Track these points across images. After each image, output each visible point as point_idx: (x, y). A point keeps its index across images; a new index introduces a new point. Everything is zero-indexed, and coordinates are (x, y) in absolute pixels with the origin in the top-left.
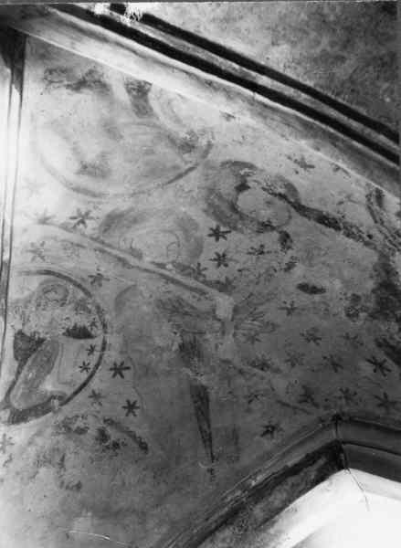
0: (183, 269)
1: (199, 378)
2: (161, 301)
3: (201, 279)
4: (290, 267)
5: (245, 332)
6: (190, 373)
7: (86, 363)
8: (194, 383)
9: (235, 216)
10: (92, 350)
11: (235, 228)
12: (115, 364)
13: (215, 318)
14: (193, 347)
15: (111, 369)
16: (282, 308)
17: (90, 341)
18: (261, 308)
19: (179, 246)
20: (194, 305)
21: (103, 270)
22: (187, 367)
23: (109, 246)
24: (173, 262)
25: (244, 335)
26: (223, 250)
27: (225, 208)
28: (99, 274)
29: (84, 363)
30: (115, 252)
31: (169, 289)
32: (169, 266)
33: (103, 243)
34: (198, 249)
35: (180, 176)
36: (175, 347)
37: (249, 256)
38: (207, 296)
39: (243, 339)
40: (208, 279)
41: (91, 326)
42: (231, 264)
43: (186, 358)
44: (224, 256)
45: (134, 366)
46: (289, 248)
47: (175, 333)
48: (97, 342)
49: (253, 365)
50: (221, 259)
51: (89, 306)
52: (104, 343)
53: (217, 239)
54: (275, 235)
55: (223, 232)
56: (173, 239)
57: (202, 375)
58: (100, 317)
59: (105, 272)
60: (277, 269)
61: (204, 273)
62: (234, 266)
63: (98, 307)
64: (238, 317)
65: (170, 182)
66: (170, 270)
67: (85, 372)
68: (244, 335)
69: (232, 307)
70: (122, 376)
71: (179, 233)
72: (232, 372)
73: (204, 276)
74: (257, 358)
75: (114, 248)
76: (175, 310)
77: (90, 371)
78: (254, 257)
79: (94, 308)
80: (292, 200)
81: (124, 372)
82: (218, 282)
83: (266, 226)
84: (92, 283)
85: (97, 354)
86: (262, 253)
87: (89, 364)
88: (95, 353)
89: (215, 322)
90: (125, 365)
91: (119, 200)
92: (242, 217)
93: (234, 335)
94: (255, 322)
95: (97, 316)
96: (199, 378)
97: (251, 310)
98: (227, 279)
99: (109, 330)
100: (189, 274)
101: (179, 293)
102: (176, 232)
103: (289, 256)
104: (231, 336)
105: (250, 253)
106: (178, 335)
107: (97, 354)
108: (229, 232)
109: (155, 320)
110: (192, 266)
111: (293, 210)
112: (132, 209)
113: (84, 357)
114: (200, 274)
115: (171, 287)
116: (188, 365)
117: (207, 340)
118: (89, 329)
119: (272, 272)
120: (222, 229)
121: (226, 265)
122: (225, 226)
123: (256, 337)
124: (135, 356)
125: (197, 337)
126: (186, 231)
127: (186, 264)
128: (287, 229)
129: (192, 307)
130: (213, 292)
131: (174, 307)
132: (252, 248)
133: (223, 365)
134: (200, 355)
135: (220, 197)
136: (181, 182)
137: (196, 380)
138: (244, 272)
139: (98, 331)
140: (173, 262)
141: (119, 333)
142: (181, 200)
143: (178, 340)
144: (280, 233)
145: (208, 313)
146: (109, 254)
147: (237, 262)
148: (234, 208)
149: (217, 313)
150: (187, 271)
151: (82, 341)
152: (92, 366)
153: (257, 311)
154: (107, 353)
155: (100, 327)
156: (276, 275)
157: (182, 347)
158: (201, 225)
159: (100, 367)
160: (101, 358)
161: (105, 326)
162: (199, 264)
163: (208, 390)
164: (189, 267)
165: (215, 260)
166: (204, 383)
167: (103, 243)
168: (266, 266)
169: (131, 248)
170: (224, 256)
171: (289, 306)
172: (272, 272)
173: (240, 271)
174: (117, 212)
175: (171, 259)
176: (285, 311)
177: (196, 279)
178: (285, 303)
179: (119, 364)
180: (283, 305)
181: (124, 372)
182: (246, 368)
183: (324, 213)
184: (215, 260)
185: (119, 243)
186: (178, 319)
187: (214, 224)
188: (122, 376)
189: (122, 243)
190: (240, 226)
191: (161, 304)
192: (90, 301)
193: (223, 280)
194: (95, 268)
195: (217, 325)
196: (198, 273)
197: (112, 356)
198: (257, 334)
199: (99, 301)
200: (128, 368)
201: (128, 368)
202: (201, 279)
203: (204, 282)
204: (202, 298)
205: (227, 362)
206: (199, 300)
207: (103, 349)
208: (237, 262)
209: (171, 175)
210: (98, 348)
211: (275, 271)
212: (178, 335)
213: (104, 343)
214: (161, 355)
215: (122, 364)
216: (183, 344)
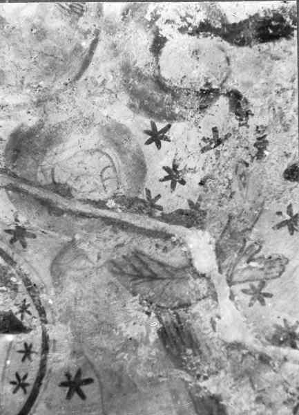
0: (130, 203)
1: (202, 384)
2: (113, 262)
3: (158, 213)
4: (261, 144)
5: (247, 286)
6: (188, 378)
7: (22, 375)
8: (201, 394)
9: (168, 96)
10: (27, 351)
11: (173, 118)
12: (68, 375)
13: (198, 275)
14: (178, 330)
15: (63, 384)
16: (280, 226)
17: (24, 337)
18: (252, 237)
19: (115, 170)
20: (161, 259)
21: (22, 219)
22: (181, 367)
23: (25, 181)
24: (114, 197)
25: (244, 291)
26: (171, 160)
27: (149, 88)
28: (18, 227)
29: (17, 375)
30: (34, 191)
31: (120, 241)
32: (111, 203)
33: (15, 176)
34: (140, 167)
35: (86, 64)
36: (153, 337)
37: (204, 155)
38: (174, 239)
39: (247, 298)
40: (166, 211)
41: (21, 311)
42: (187, 176)
43: (175, 351)
44: (175, 167)
45: (98, 376)
46: (247, 114)
47: (148, 314)
48: (34, 338)
49: (276, 341)
50: (174, 175)
51: (13, 279)
52: (45, 338)
53: (159, 145)
54: (223, 102)
55: (161, 132)
56: (104, 161)
57: (206, 378)
58: (33, 297)
59: (28, 223)
60: (248, 161)
61: (158, 203)
62: (193, 179)
63: (27, 281)
64: (226, 263)
65: (78, 77)
66: (113, 209)
67: (21, 391)
68: (244, 291)
69: (212, 247)
70: (83, 397)
71: (111, 151)
72: (250, 363)
73: (160, 208)
74: (278, 327)
75: (31, 184)
76: (137, 275)
77: (29, 389)
78: (211, 153)
79: (20, 283)
80: (219, 26)
81: (84, 388)
82: (181, 212)
83: (207, 95)
84: (12, 241)
85: (36, 358)
86: (219, 142)
87: (25, 377)
88: (33, 356)
89: (198, 281)
90: (84, 377)
91: (24, 112)
92: (175, 93)
93: (232, 297)
94: (252, 264)
95: (27, 297)
96: (202, 384)
97: (240, 245)
98: (191, 203)
99: (49, 316)
100: (140, 211)
101: (135, 244)
102: (107, 151)
103: (252, 128)
104: (227, 300)
105: (203, 150)
106: (153, 314)
107: (36, 358)
108: (169, 126)
109: (114, 295)
110: (141, 197)
111: (226, 44)
112: (41, 125)
113: (14, 363)
114: (153, 206)
115: (123, 236)
116: (181, 365)
117: (195, 316)
118: (19, 316)
119: (243, 169)
120: (160, 126)
121: (183, 182)
122: (160, 121)
123: (264, 291)
124: (98, 360)
125: (181, 312)
126: (117, 145)
127: (132, 195)
128: (230, 85)
129: (161, 264)
130: (177, 230)
131: (135, 269)
132: (204, 139)
133: (234, 353)
134: (194, 345)
135: (139, 75)
136: (90, 72)
137: (199, 389)
138: (209, 183)
139: (31, 319)
140: (114, 197)
141: (65, 322)
142: (97, 99)
143: (156, 325)
144: (228, 94)
145: (184, 268)
146: (27, 193)
147: (194, 171)
148: (160, 84)
149: (196, 264)
150: (136, 206)
151: (10, 338)
152: (31, 380)
153: (248, 244)
154: (51, 355)
155: (35, 313)
156: (251, 168)
157: (163, 334)
158: (133, 131)
159: (44, 381)
160: (43, 365)
161: (42, 312)
162: (148, 192)
163: (224, 403)
164: (137, 199)
165: (166, 179)
166: (214, 391)
167: (15, 176)
168: (232, 163)
169: (55, 183)
170: (175, 167)
171: (288, 217)
172: (243, 169)
173: (202, 183)
174: (25, 129)
175: (110, 192)
176: (285, 229)
177: (150, 215)
178: (279, 213)
179: (73, 374)
180: (280, 219)
181: (84, 388)
182: (270, 350)
183: (262, 15)
184: (166, 179)
185: (35, 175)
186: (143, 287)
187: (146, 122)
188: (83, 397)
189: (40, 177)
190: (177, 111)
191: (116, 268)
192: (13, 271)
193: (185, 206)
194: (11, 217)
195: (202, 285)
196: (149, 206)
197: (61, 360)
198: (263, 284)
199: (25, 269)
200: (89, 381)
201: (89, 381)
202: (158, 213)
203: (164, 218)
204: (169, 244)
205: (237, 346)
206: (165, 250)
207: (45, 349)
208: (194, 171)
209: (76, 64)
210: (37, 347)
211: (247, 165)
212: (153, 314)
213: (45, 338)
214: (135, 352)
215: (79, 373)
216: (163, 328)
